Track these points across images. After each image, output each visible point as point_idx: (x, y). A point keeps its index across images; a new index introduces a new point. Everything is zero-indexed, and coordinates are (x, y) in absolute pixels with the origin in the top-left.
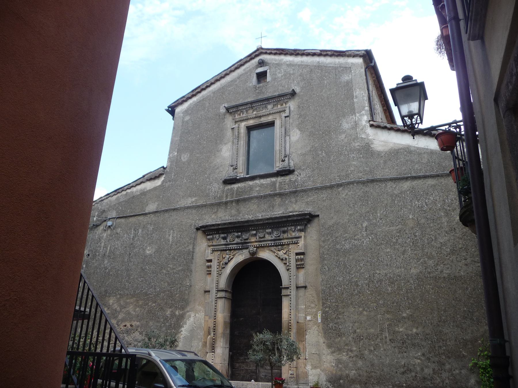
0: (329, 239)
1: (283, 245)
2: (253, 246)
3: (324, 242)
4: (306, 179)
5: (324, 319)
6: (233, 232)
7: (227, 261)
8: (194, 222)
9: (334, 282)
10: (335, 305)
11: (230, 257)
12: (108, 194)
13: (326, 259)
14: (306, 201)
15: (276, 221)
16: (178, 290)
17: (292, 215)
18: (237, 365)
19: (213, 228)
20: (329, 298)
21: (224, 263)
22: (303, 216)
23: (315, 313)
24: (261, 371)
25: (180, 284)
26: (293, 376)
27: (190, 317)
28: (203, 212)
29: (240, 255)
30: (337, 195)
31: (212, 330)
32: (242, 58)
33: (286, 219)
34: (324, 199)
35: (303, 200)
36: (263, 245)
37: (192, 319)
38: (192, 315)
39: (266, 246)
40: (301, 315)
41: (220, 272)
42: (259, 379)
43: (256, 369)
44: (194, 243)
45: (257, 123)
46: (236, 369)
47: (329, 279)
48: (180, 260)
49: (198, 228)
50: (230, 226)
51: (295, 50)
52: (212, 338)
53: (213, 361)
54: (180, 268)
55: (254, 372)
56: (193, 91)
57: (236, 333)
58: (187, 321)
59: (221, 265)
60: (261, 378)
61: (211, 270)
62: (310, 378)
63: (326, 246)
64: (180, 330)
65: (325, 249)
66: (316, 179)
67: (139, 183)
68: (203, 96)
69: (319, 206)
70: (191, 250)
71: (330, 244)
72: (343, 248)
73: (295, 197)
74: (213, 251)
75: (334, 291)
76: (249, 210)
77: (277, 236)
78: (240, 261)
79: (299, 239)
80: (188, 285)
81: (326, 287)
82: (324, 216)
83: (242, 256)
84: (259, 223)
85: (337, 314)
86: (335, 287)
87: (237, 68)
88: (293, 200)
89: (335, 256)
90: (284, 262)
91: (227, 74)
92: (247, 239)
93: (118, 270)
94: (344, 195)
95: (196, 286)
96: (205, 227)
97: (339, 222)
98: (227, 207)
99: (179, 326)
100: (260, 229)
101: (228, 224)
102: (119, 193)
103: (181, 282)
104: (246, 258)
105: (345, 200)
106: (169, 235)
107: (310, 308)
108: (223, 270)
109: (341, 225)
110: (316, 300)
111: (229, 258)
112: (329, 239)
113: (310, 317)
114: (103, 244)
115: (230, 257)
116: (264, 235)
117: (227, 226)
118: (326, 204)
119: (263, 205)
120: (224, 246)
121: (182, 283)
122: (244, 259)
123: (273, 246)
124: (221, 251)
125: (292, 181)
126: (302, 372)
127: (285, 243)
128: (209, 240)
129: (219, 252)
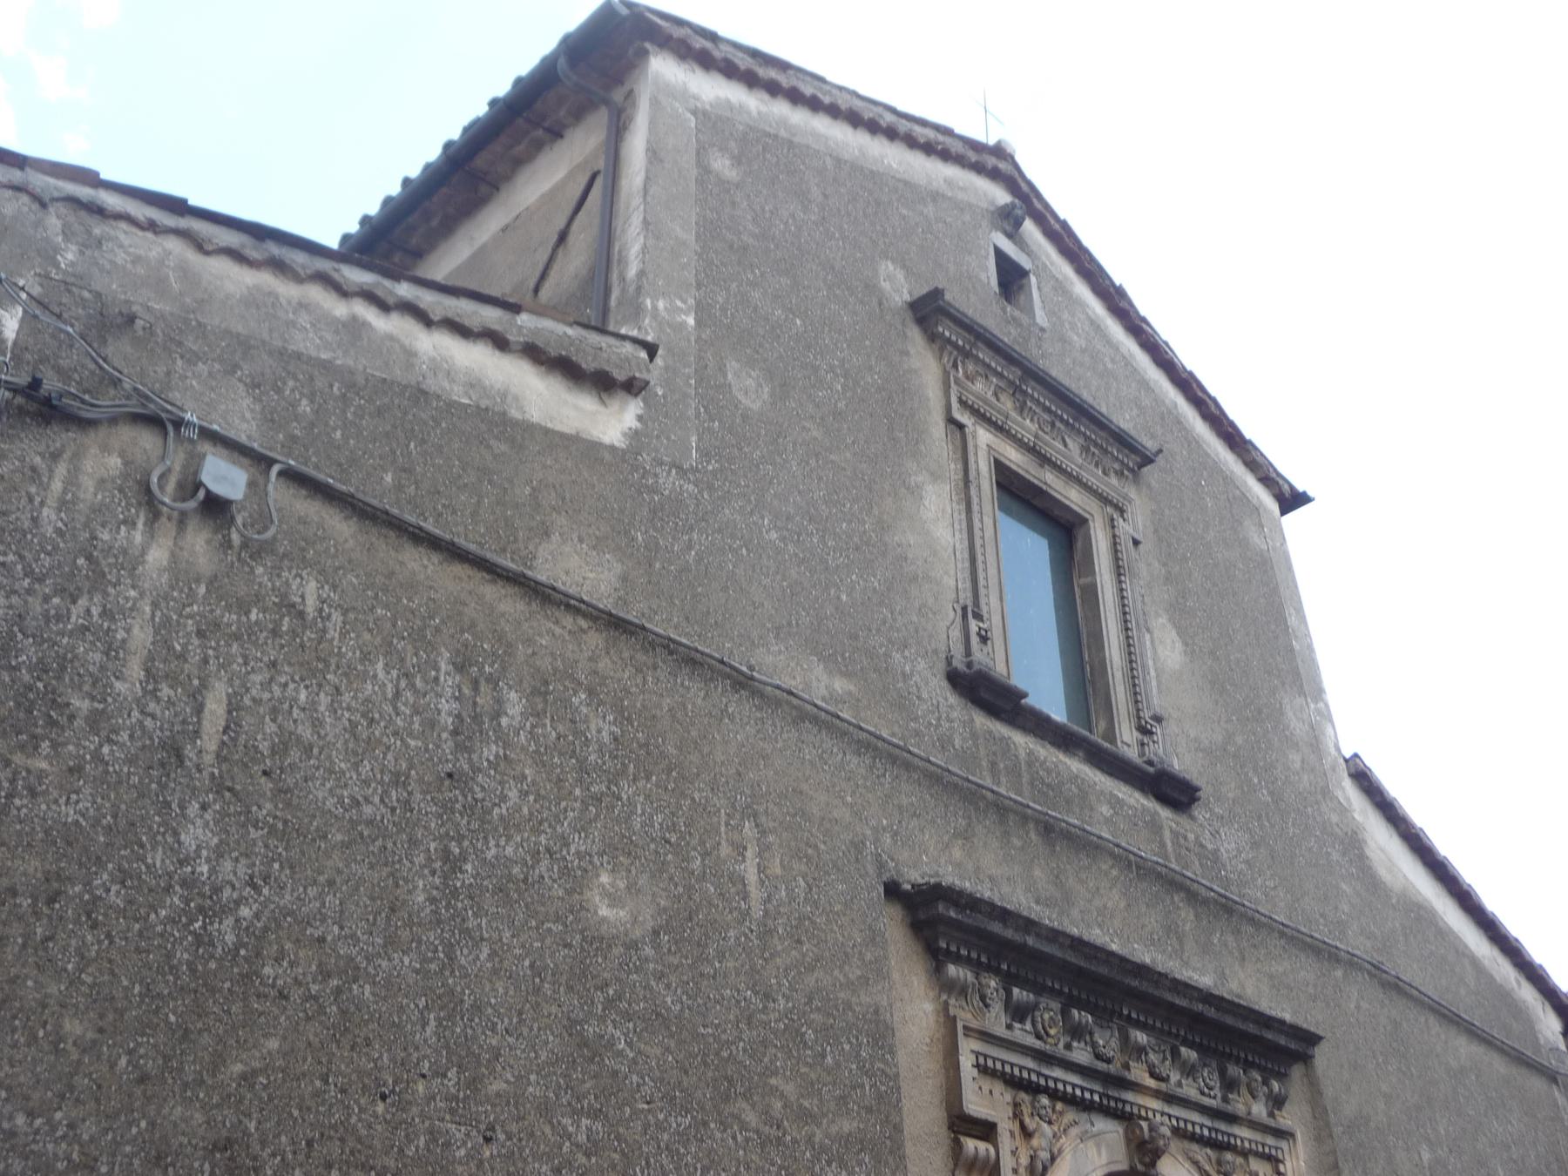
12: (177, 206)
19: (996, 927)
32: (958, 130)
45: (1027, 476)
50: (1071, 957)
51: (1121, 292)
54: (847, 1126)
56: (755, 54)
67: (473, 324)
68: (783, 122)
87: (929, 149)
91: (891, 134)
93: (351, 972)
101: (1068, 942)
102: (278, 266)
106: (740, 850)
114: (140, 636)
117: (1058, 953)
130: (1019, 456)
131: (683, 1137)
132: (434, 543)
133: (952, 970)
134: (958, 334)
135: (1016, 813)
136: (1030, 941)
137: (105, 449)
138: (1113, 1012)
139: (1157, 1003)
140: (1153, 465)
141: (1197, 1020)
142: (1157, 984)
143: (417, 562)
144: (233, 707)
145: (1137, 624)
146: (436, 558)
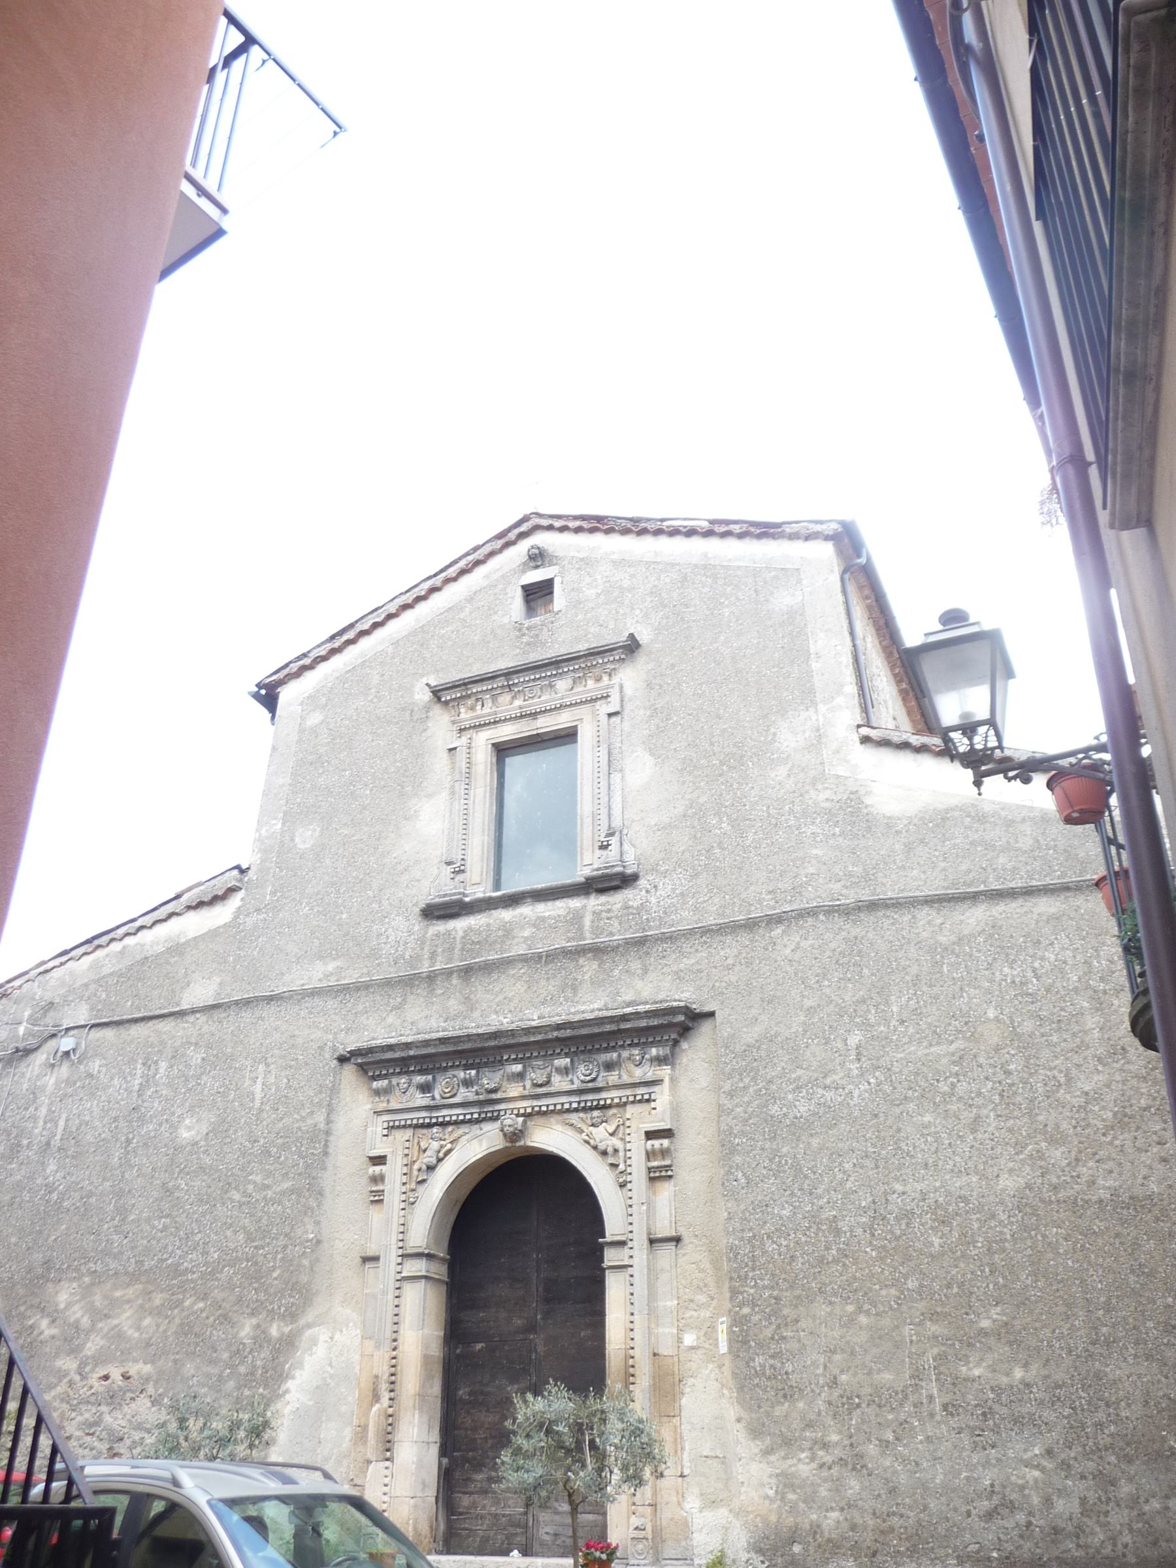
1: (605, 1107)
5: (737, 1341)
6: (451, 1067)
10: (770, 1296)
11: (442, 1147)
13: (739, 1148)
14: (675, 968)
18: (465, 1501)
19: (389, 1055)
20: (751, 1274)
21: (424, 1167)
22: (665, 1015)
23: (709, 1324)
24: (541, 1519)
28: (360, 1007)
30: (767, 949)
31: (384, 1387)
33: (613, 1027)
34: (730, 961)
37: (320, 1351)
40: (667, 1330)
42: (536, 1547)
43: (526, 1513)
46: (461, 1514)
48: (287, 1158)
50: (443, 1049)
52: (386, 1411)
53: (386, 1489)
54: (286, 1185)
57: (461, 1392)
58: (307, 1358)
59: (415, 1173)
60: (542, 1544)
62: (698, 1538)
63: (739, 1110)
64: (283, 1388)
65: (733, 1119)
66: (705, 902)
69: (714, 986)
71: (749, 1103)
72: (791, 1116)
75: (764, 1253)
79: (656, 1089)
81: (742, 1239)
82: (729, 1015)
83: (481, 1145)
85: (779, 1327)
88: (636, 965)
90: (611, 1160)
93: (90, 1194)
94: (788, 951)
97: (777, 1035)
98: (434, 989)
99: (281, 1375)
100: (536, 1057)
103: (287, 1230)
108: (421, 1189)
110: (710, 1280)
113: (695, 1337)
115: (442, 1147)
116: (549, 1076)
117: (433, 1051)
119: (543, 983)
120: (424, 1114)
123: (576, 1110)
125: (632, 907)
126: (672, 1519)
128: (377, 1093)
129: (409, 1133)
130: (515, 727)
131: (204, 1214)
132: (136, 1021)
134: (549, 670)
136: (412, 1053)
137: (42, 1054)
140: (636, 635)
143: (136, 1031)
144: (67, 1120)
145: (474, 802)
146: (142, 1024)
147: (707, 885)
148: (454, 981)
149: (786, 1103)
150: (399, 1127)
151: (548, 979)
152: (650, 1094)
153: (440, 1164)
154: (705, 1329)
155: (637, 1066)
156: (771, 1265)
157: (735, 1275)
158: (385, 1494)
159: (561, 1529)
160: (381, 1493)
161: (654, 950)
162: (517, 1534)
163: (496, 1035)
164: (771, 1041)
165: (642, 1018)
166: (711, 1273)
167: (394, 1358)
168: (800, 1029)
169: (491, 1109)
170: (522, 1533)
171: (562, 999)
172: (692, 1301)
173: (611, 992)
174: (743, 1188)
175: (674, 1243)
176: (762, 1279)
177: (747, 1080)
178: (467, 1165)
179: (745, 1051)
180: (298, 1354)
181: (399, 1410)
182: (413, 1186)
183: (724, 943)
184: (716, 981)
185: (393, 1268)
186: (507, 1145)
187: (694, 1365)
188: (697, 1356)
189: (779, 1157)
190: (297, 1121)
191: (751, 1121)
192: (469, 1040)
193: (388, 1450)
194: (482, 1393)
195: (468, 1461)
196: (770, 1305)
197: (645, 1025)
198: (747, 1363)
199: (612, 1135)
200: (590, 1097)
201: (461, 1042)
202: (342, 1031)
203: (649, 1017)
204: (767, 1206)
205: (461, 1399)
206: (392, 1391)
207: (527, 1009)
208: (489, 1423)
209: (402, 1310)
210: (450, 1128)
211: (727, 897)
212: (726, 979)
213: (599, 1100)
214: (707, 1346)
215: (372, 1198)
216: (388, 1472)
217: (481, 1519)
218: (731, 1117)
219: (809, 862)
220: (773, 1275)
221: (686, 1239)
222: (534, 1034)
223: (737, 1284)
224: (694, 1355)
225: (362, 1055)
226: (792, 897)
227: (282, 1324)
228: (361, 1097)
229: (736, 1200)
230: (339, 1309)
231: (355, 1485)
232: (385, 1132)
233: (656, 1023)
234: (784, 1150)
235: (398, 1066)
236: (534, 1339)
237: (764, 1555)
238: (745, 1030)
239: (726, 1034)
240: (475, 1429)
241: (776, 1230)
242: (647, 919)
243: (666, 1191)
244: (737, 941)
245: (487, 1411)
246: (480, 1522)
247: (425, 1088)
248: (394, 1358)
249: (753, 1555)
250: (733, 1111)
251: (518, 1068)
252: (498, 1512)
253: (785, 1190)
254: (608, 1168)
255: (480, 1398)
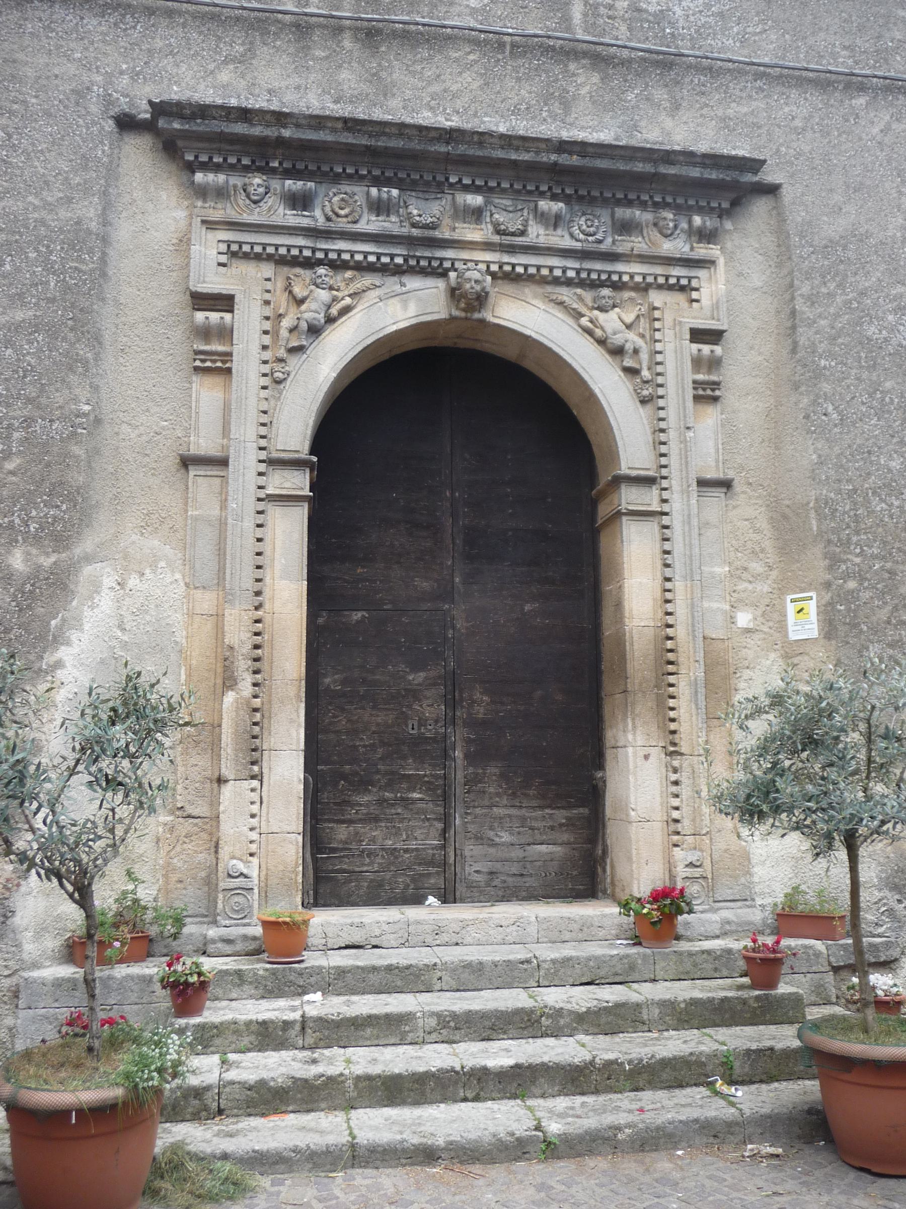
0: (831, 295)
1: (617, 286)
2: (483, 267)
3: (813, 303)
4: (711, 19)
5: (845, 624)
6: (350, 177)
7: (321, 317)
8: (99, 78)
9: (869, 474)
10: (882, 568)
11: (335, 299)
13: (828, 373)
14: (720, 113)
15: (602, 164)
16: (16, 435)
17: (625, 171)
18: (342, 832)
19: (240, 128)
20: (855, 539)
21: (304, 326)
22: (729, 167)
23: (767, 601)
24: (467, 853)
25: (29, 400)
26: (697, 872)
27: (99, 593)
28: (159, 43)
29: (395, 301)
30: (847, 120)
31: (242, 666)
33: (649, 168)
34: (798, 123)
35: (707, 105)
36: (520, 270)
37: (106, 602)
38: (108, 581)
39: (530, 279)
40: (715, 605)
41: (278, 366)
42: (461, 889)
43: (444, 847)
44: (105, 193)
46: (334, 850)
47: (848, 461)
48: (18, 270)
49: (126, 115)
50: (348, 138)
52: (248, 703)
53: (254, 822)
55: (431, 863)
57: (327, 680)
58: (87, 612)
59: (284, 333)
60: (470, 886)
61: (230, 354)
62: (760, 872)
63: (823, 322)
64: (49, 658)
65: (816, 333)
66: (756, 34)
69: (778, 150)
70: (94, 226)
71: (837, 316)
72: (894, 342)
73: (666, 86)
74: (236, 254)
75: (871, 513)
76: (436, 88)
77: (590, 239)
78: (394, 328)
79: (702, 273)
80: (85, 415)
81: (839, 492)
82: (803, 194)
83: (405, 307)
84: (514, 156)
85: (896, 608)
86: (874, 493)
88: (660, 94)
89: (861, 367)
90: (629, 362)
92: (433, 227)
94: (875, 130)
95: (125, 428)
96: (192, 117)
97: (868, 235)
98: (309, 48)
99: (42, 637)
100: (504, 191)
101: (340, 125)
103: (31, 391)
104: (429, 318)
105: (882, 150)
107: (745, 575)
108: (294, 362)
109: (875, 246)
110: (768, 544)
111: (329, 307)
112: (831, 295)
113: (750, 616)
115: (335, 299)
116: (525, 224)
117: (330, 138)
118: (807, 148)
119: (510, 83)
120: (301, 241)
121: (43, 400)
122: (414, 321)
123: (569, 283)
124: (281, 261)
125: (646, 11)
126: (726, 851)
127: (632, 277)
128: (202, 192)
129: (268, 270)
133: (199, 177)
135: (324, 27)
136: (286, 133)
138: (440, 185)
139: (499, 164)
141: (555, 170)
142: (481, 144)
147: (758, 14)
148: (347, 43)
149: (885, 324)
150: (246, 256)
151: (519, 79)
152: (690, 279)
153: (330, 328)
154: (762, 608)
155: (666, 236)
156: (880, 530)
157: (834, 538)
158: (252, 829)
159: (498, 866)
160: (246, 829)
161: (687, 80)
162: (429, 875)
163: (451, 135)
164: (861, 241)
165: (694, 165)
166: (769, 535)
167: (258, 621)
168: (899, 234)
169: (428, 254)
170: (438, 873)
171: (544, 114)
172: (746, 569)
173: (624, 122)
174: (836, 426)
175: (724, 490)
176: (870, 547)
177: (832, 286)
178: (381, 335)
179: (826, 247)
180: (74, 603)
181: (270, 702)
182: (282, 353)
183: (788, 97)
184: (781, 145)
185: (252, 480)
186: (456, 313)
187: (750, 654)
188: (753, 641)
189: (882, 392)
190: (36, 208)
191: (840, 340)
192: (401, 135)
193: (253, 763)
194: (364, 681)
195: (344, 777)
196: (883, 580)
197: (698, 175)
198: (860, 651)
199: (629, 327)
200: (598, 266)
201: (384, 134)
202: (122, 73)
203: (704, 166)
204: (869, 452)
205: (328, 688)
206: (256, 672)
207: (486, 115)
208: (378, 724)
209: (266, 547)
210: (349, 274)
211: (787, 36)
212: (794, 145)
213: (610, 273)
214: (766, 630)
215: (198, 363)
216: (255, 796)
217: (369, 856)
218: (813, 330)
219: (895, 24)
220: (885, 543)
221: (738, 487)
222: (517, 149)
223: (838, 550)
224: (749, 640)
225: (182, 117)
226: (876, 62)
227: (34, 551)
228: (164, 195)
229: (827, 440)
230: (134, 537)
231: (189, 816)
232: (223, 259)
233: (714, 176)
234: (888, 385)
235: (247, 154)
236: (449, 610)
237: (900, 893)
238: (825, 219)
239: (799, 219)
240: (354, 733)
241: (884, 485)
242: (672, 34)
243: (711, 417)
244: (806, 99)
245: (373, 708)
246: (368, 860)
247: (300, 202)
248: (258, 621)
249: (886, 893)
250: (815, 322)
251: (477, 200)
252: (398, 846)
253: (893, 436)
254: (622, 374)
255: (362, 690)
